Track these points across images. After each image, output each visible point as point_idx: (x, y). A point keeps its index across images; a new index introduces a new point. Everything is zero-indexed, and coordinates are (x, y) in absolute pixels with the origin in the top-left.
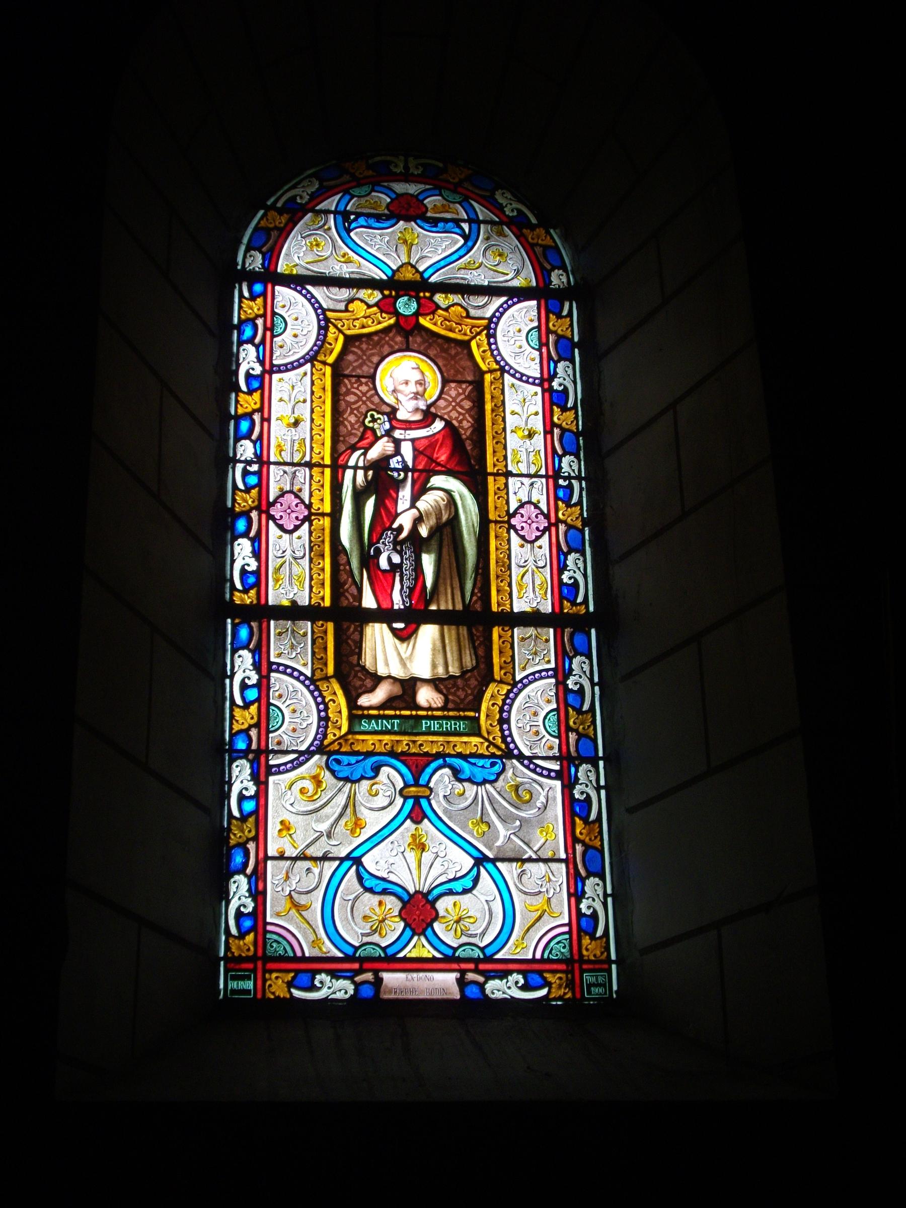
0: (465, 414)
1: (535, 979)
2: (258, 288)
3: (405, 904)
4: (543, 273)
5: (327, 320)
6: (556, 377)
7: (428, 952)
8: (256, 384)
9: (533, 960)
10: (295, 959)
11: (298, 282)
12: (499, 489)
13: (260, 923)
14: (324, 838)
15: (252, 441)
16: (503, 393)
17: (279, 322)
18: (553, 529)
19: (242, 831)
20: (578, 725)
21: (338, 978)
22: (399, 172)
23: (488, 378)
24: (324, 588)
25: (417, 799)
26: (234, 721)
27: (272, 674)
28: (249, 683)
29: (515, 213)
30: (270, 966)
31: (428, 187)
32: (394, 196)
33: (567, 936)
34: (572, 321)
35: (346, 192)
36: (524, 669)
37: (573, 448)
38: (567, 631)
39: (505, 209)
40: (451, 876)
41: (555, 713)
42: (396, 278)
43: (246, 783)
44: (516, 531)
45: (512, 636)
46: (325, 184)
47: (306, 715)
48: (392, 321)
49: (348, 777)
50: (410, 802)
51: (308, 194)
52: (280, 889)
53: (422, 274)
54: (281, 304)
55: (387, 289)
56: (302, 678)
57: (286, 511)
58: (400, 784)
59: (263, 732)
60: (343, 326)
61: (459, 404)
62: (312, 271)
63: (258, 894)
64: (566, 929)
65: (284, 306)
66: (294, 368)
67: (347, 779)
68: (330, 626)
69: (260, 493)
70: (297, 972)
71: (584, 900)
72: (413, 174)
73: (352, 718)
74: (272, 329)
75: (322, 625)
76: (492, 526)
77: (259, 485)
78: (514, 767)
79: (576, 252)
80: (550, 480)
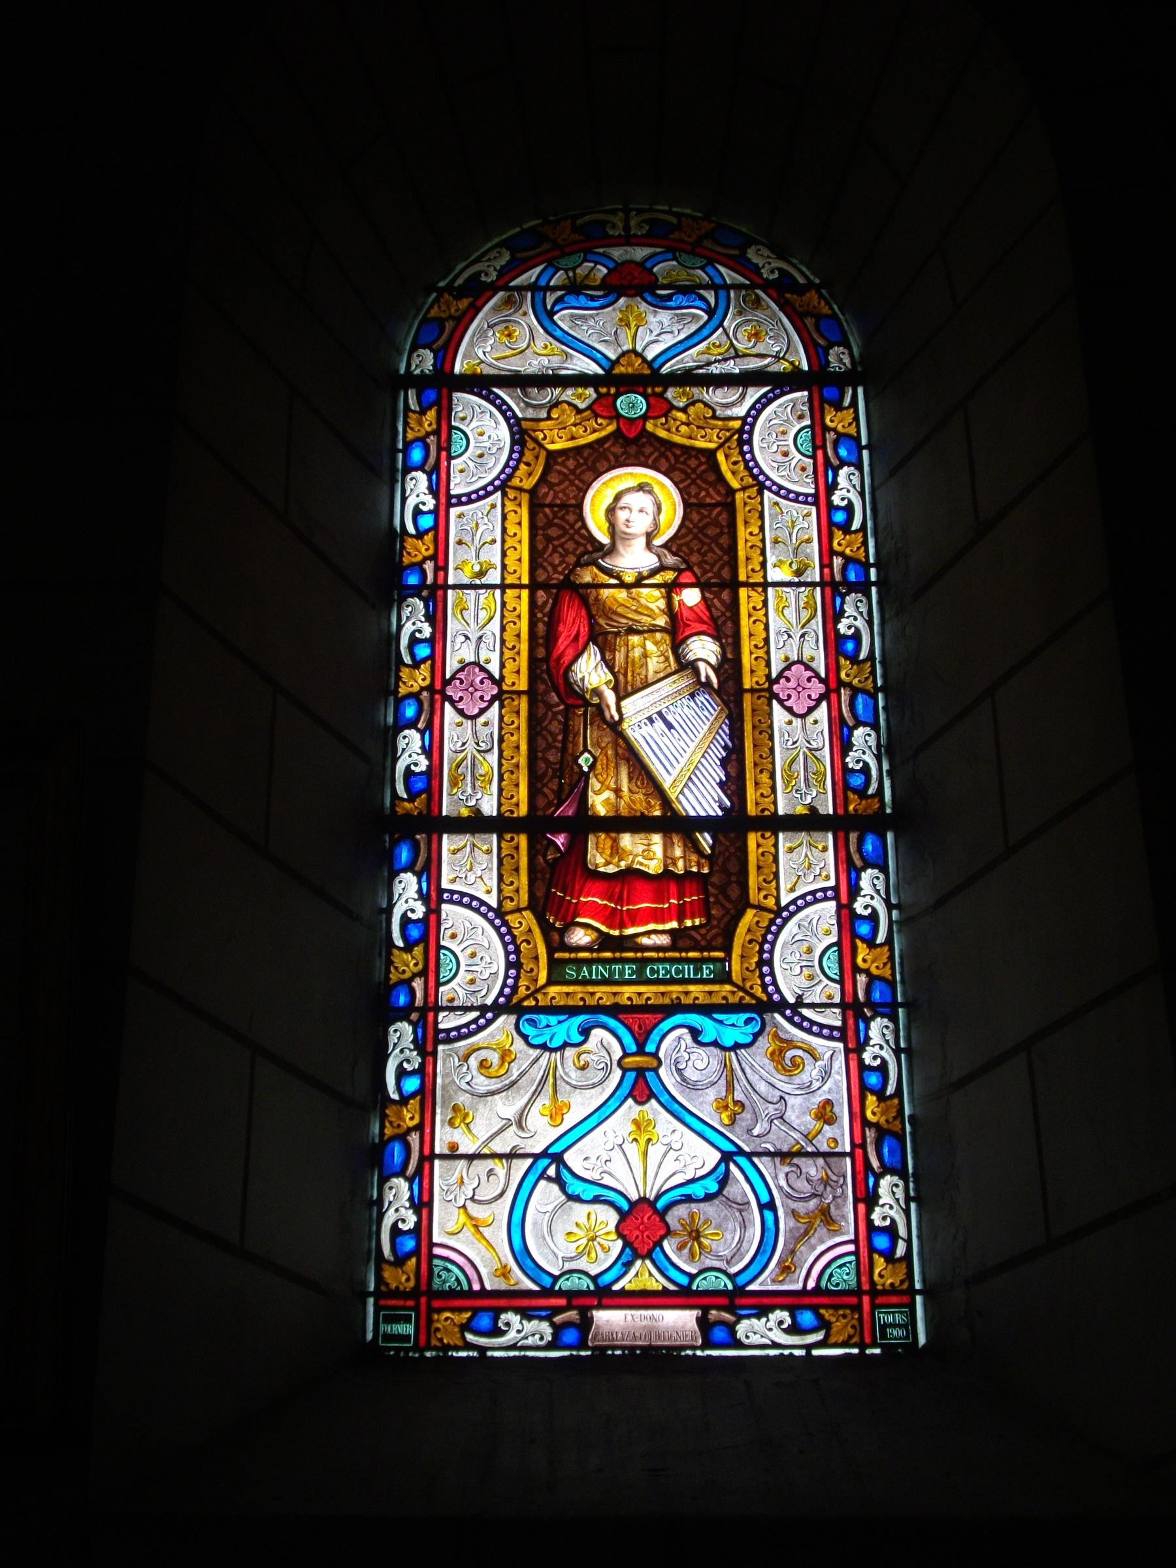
0: (711, 543)
1: (807, 1318)
2: (431, 395)
3: (623, 1216)
4: (816, 352)
5: (523, 432)
6: (869, 1045)
7: (656, 1282)
8: (415, 933)
9: (804, 1292)
10: (471, 1293)
11: (480, 384)
12: (756, 646)
13: (424, 1244)
14: (514, 1128)
15: (418, 730)
16: (776, 860)
17: (448, 961)
18: (833, 696)
19: (421, 424)
20: (852, 677)
21: (530, 1318)
22: (617, 234)
23: (739, 496)
24: (518, 875)
25: (641, 1051)
26: (400, 684)
27: (444, 907)
28: (424, 508)
29: (776, 275)
30: (436, 1304)
31: (658, 250)
32: (611, 265)
33: (852, 1258)
34: (856, 412)
35: (550, 264)
36: (792, 890)
37: (895, 1162)
38: (853, 837)
39: (762, 271)
40: (689, 1176)
41: (836, 948)
42: (616, 371)
43: (412, 903)
44: (781, 702)
45: (776, 845)
46: (519, 255)
47: (496, 438)
48: (611, 428)
49: (545, 1043)
50: (631, 1076)
51: (495, 269)
52: (451, 1197)
53: (650, 364)
54: (461, 415)
55: (603, 386)
56: (483, 909)
57: (467, 690)
58: (617, 1053)
59: (432, 984)
60: (545, 438)
61: (699, 476)
62: (503, 370)
63: (422, 1204)
64: (851, 1248)
65: (463, 419)
66: (480, 498)
67: (544, 1047)
68: (523, 840)
69: (433, 667)
70: (476, 1311)
71: (859, 899)
72: (635, 236)
73: (553, 963)
74: (448, 450)
75: (512, 839)
76: (747, 697)
77: (435, 528)
78: (776, 1025)
79: (864, 348)
80: (851, 1000)
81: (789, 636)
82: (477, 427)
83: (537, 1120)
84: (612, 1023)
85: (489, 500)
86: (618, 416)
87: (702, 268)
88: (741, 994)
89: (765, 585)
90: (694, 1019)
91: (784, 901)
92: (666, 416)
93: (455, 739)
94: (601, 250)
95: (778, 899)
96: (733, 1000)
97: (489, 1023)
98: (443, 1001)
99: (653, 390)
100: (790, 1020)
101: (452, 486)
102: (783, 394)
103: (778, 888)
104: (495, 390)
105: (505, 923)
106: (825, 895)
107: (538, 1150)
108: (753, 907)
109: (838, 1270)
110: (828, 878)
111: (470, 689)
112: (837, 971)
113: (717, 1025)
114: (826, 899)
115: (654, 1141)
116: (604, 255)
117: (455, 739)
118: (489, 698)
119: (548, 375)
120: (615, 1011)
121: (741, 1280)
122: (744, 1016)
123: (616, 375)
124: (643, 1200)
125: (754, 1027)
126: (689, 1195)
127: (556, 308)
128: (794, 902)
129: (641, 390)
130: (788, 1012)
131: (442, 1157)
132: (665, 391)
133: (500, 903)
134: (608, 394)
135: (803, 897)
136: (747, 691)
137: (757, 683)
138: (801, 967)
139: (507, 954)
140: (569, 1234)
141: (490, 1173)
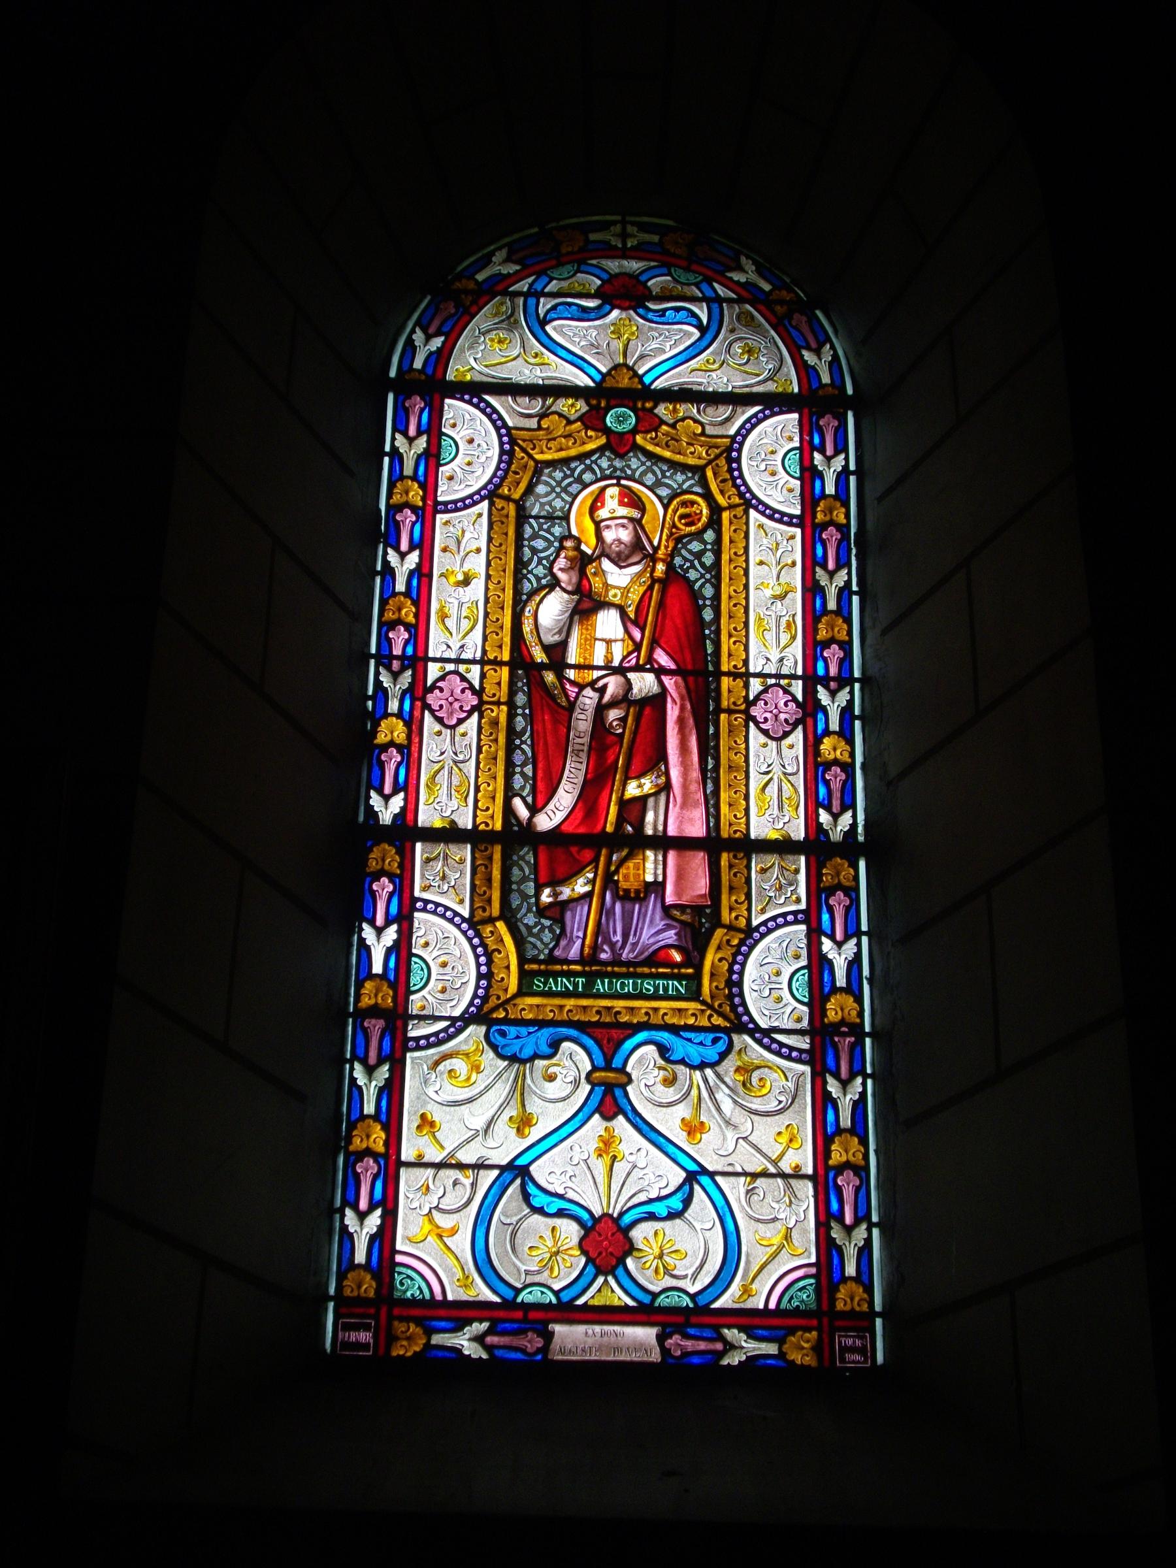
31: (653, 264)
36: (763, 911)
50: (599, 1090)
86: (607, 431)
87: (697, 285)
90: (664, 1037)
95: (749, 920)
97: (459, 1031)
98: (414, 1009)
99: (643, 405)
100: (759, 1042)
101: (439, 494)
102: (773, 414)
104: (487, 397)
107: (504, 1162)
108: (724, 926)
122: (711, 1036)
124: (606, 1215)
125: (721, 1046)
127: (552, 315)
128: (764, 923)
132: (655, 406)
135: (774, 918)
137: (735, 666)
138: (770, 989)
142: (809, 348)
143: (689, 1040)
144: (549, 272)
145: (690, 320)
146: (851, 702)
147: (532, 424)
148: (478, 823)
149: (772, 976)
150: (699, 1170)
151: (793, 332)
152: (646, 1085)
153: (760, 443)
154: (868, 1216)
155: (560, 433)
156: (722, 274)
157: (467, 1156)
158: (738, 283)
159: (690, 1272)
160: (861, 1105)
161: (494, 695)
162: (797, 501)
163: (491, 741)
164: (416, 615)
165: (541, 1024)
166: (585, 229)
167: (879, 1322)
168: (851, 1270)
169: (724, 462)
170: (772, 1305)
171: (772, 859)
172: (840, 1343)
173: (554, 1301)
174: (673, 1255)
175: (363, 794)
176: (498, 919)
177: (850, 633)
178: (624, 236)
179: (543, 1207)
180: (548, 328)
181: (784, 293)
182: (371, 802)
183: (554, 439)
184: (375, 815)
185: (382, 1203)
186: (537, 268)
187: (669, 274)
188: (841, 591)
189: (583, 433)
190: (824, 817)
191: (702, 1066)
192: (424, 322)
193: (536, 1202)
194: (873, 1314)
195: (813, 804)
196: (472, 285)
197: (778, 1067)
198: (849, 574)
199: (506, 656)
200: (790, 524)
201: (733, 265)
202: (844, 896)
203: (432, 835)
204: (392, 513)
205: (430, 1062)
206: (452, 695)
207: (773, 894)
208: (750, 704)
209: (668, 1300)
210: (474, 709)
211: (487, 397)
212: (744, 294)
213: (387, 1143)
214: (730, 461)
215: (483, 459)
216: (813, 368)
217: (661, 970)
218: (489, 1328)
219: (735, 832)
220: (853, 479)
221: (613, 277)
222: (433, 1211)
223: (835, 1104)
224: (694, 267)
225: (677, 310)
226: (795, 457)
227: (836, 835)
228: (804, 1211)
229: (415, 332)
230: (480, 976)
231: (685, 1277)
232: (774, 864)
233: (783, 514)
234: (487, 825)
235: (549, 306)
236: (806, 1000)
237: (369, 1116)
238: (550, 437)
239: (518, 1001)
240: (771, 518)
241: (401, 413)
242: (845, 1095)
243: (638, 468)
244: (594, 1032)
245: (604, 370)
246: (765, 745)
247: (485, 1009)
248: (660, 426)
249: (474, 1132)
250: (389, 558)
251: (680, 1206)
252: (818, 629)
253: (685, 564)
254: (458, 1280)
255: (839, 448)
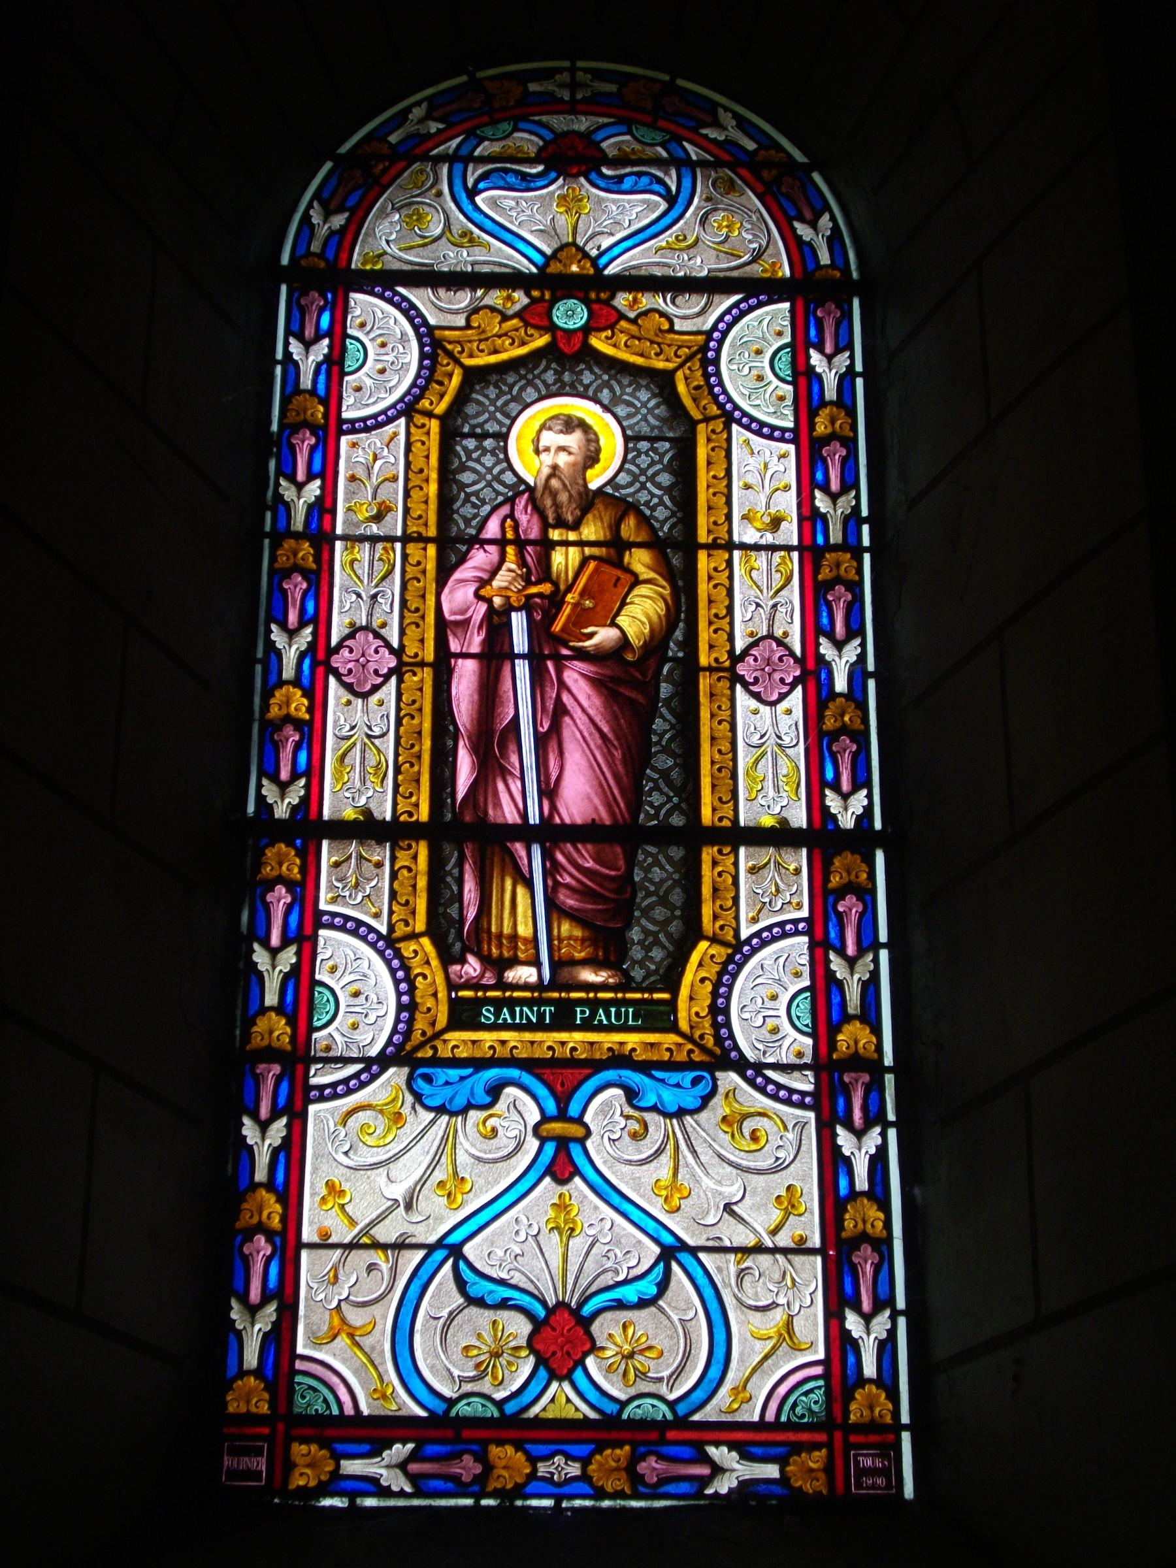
31: (606, 120)
32: (549, 136)
33: (821, 1383)
36: (755, 920)
41: (808, 994)
45: (736, 864)
50: (550, 1148)
55: (536, 288)
58: (534, 1116)
60: (462, 352)
64: (818, 1370)
67: (440, 1110)
81: (758, 605)
82: (380, 335)
83: (431, 1201)
84: (527, 1079)
85: (389, 429)
86: (552, 328)
87: (663, 145)
88: (690, 1046)
89: (730, 546)
90: (635, 1078)
91: (745, 933)
92: (612, 327)
93: (342, 722)
94: (536, 118)
95: (737, 931)
96: (681, 1057)
97: (374, 1078)
98: (317, 1049)
99: (598, 296)
100: (751, 1082)
101: (344, 408)
102: (760, 305)
103: (737, 918)
104: (400, 289)
105: (398, 954)
106: (796, 928)
107: (432, 1239)
108: (707, 938)
109: (804, 1398)
110: (799, 906)
111: (362, 660)
112: (808, 1021)
113: (658, 1084)
114: (797, 933)
115: (577, 1232)
116: (540, 124)
117: (342, 722)
118: (385, 671)
119: (467, 273)
120: (528, 1065)
121: (681, 1409)
122: (690, 1076)
123: (552, 275)
124: (561, 1305)
125: (703, 1089)
126: (618, 1301)
127: (481, 186)
128: (758, 934)
129: (581, 295)
130: (749, 1072)
131: (312, 1246)
132: (613, 297)
133: (391, 928)
134: (541, 299)
135: (769, 928)
136: (704, 669)
137: (716, 660)
138: (764, 1017)
139: (399, 994)
140: (467, 1348)
141: (372, 1268)
142: (802, 220)
143: (662, 1081)
144: (478, 132)
145: (656, 187)
146: (862, 657)
147: (460, 321)
148: (394, 921)
149: (766, 999)
150: (678, 1245)
151: (784, 202)
152: (609, 1139)
153: (742, 341)
154: (891, 1301)
155: (494, 332)
156: (695, 130)
157: (387, 1233)
158: (714, 141)
159: (665, 1374)
160: (889, 1346)
161: (416, 655)
162: (789, 412)
163: (412, 755)
164: (310, 710)
165: (479, 1064)
166: (523, 78)
167: (906, 1437)
168: (870, 1369)
169: (698, 365)
170: (770, 1416)
171: (767, 854)
172: (857, 1463)
173: (496, 1414)
174: (647, 1354)
175: (262, 629)
176: (421, 935)
177: (854, 427)
178: (573, 86)
179: (483, 1297)
180: (478, 200)
181: (773, 152)
182: (273, 637)
183: (487, 339)
184: (270, 808)
185: (307, 773)
186: (467, 125)
187: (630, 132)
188: (846, 520)
189: (522, 331)
190: (832, 801)
191: (680, 1113)
192: (325, 195)
193: (473, 1291)
194: (898, 1427)
195: (816, 785)
196: (386, 150)
197: (778, 1116)
198: (870, 796)
199: (432, 532)
200: (782, 440)
201: (709, 120)
202: (877, 1389)
203: (341, 830)
204: (276, 580)
205: (338, 1118)
206: (363, 655)
207: (767, 900)
208: (735, 659)
209: (639, 1411)
210: (391, 672)
211: (400, 289)
212: (726, 157)
213: (284, 1219)
214: (705, 363)
215: (372, 1019)
216: (809, 244)
217: (629, 995)
218: (414, 1451)
219: (721, 819)
220: (859, 382)
221: (560, 137)
222: (343, 1304)
223: (848, 1162)
224: (661, 123)
225: (639, 175)
226: (785, 357)
227: (847, 821)
228: (811, 1294)
229: (313, 207)
230: (400, 1007)
231: (660, 1380)
232: (769, 862)
233: (774, 428)
234: (410, 814)
235: (480, 172)
236: (790, 379)
237: (260, 1185)
238: (483, 337)
239: (447, 1036)
240: (758, 433)
241: (296, 313)
242: (852, 975)
243: (591, 383)
244: (544, 1074)
245: (548, 251)
246: (756, 712)
247: (408, 1047)
248: (617, 322)
249: (390, 1203)
250: (292, 349)
251: (654, 1290)
252: (824, 717)
253: (651, 500)
254: (375, 1390)
255: (865, 945)
